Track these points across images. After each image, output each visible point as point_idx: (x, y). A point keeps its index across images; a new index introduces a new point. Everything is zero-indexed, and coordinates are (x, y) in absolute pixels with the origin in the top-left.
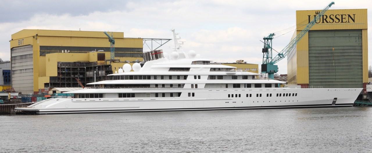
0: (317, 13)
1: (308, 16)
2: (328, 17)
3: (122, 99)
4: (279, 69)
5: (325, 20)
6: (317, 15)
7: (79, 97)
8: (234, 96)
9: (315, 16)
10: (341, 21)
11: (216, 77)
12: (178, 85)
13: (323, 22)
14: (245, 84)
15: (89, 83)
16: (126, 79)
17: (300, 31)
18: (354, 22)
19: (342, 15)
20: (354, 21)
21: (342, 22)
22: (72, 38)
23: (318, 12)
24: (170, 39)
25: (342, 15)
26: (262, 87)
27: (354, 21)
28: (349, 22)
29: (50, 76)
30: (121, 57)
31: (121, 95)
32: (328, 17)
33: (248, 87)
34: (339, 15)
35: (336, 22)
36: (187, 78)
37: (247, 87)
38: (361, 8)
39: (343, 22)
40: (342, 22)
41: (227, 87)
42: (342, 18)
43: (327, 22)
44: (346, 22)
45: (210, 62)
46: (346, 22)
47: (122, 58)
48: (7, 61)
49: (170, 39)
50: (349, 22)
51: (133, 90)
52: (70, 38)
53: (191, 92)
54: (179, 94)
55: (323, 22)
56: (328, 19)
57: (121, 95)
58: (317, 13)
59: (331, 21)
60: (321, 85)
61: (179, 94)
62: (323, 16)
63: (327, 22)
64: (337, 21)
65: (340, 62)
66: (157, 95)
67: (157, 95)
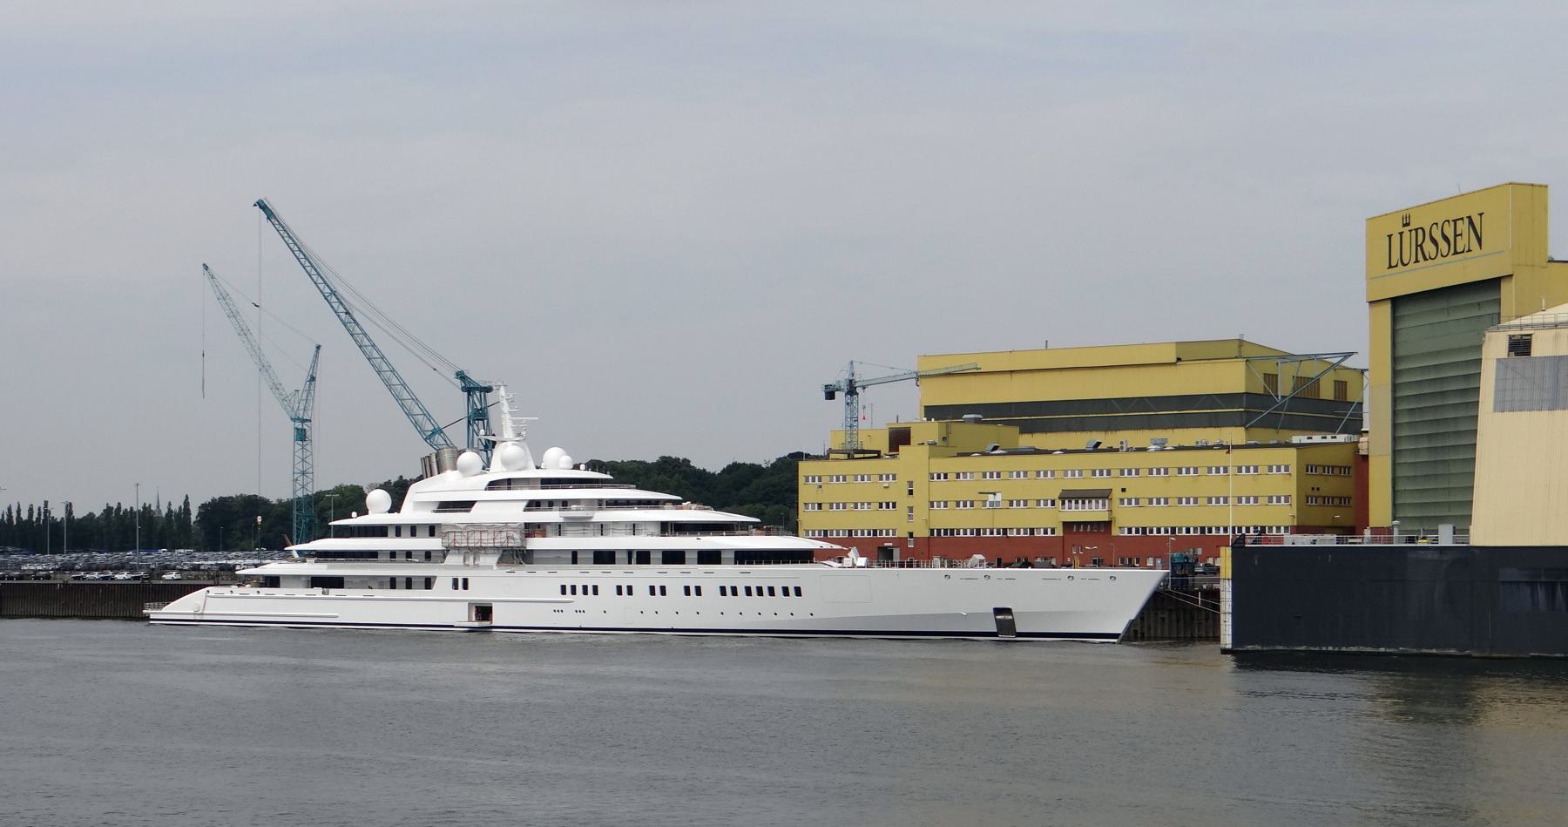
3: (318, 591)
4: (95, 513)
5: (1421, 246)
7: (1083, 566)
8: (579, 590)
9: (1401, 234)
12: (424, 553)
14: (630, 552)
16: (336, 536)
17: (1378, 301)
21: (1456, 253)
22: (1013, 375)
24: (1352, 353)
28: (1469, 250)
30: (1106, 430)
31: (316, 581)
33: (639, 562)
34: (1448, 221)
37: (637, 563)
41: (575, 561)
42: (1456, 236)
44: (1463, 252)
45: (846, 456)
46: (1463, 252)
47: (1104, 433)
49: (1352, 353)
51: (329, 568)
52: (1008, 376)
53: (461, 575)
54: (428, 583)
56: (1429, 247)
57: (316, 581)
61: (428, 583)
65: (1459, 432)
66: (393, 583)
67: (393, 583)
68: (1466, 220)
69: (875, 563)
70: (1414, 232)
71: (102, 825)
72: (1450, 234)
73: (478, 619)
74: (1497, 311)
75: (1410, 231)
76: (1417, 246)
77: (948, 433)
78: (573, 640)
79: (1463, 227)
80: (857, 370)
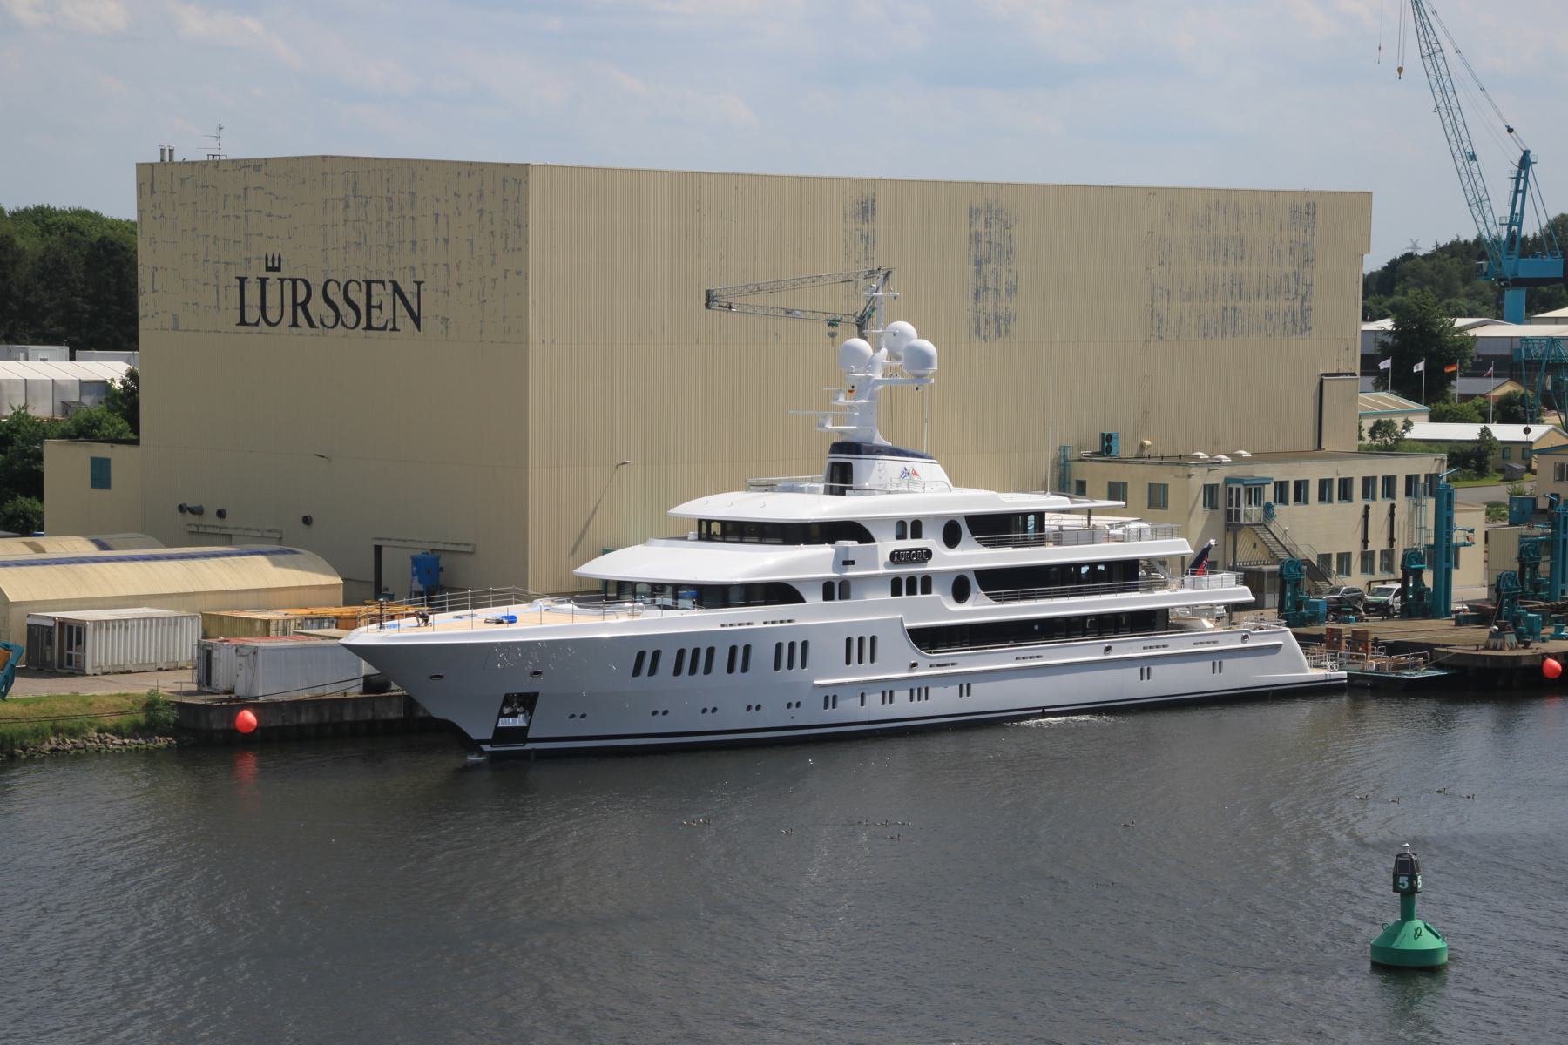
0: (270, 265)
1: (238, 282)
2: (317, 293)
6: (273, 276)
9: (263, 281)
11: (874, 451)
13: (295, 324)
15: (321, 587)
18: (419, 330)
19: (369, 283)
20: (417, 320)
21: (369, 327)
23: (276, 257)
25: (369, 283)
26: (852, 594)
27: (417, 320)
28: (394, 329)
29: (108, 491)
32: (317, 293)
34: (383, 283)
35: (343, 323)
36: (724, 494)
38: (930, 178)
39: (247, 320)
40: (369, 327)
42: (369, 307)
44: (384, 328)
46: (384, 328)
48: (77, 207)
50: (394, 329)
55: (295, 324)
56: (317, 307)
58: (270, 265)
60: (989, 545)
62: (294, 281)
64: (350, 317)
68: (389, 287)
69: (109, 382)
70: (288, 285)
71: (1378, 45)
72: (359, 298)
73: (834, 572)
74: (259, 622)
75: (282, 280)
76: (295, 304)
77: (1470, 174)
78: (250, 639)
79: (381, 294)
80: (1513, 176)
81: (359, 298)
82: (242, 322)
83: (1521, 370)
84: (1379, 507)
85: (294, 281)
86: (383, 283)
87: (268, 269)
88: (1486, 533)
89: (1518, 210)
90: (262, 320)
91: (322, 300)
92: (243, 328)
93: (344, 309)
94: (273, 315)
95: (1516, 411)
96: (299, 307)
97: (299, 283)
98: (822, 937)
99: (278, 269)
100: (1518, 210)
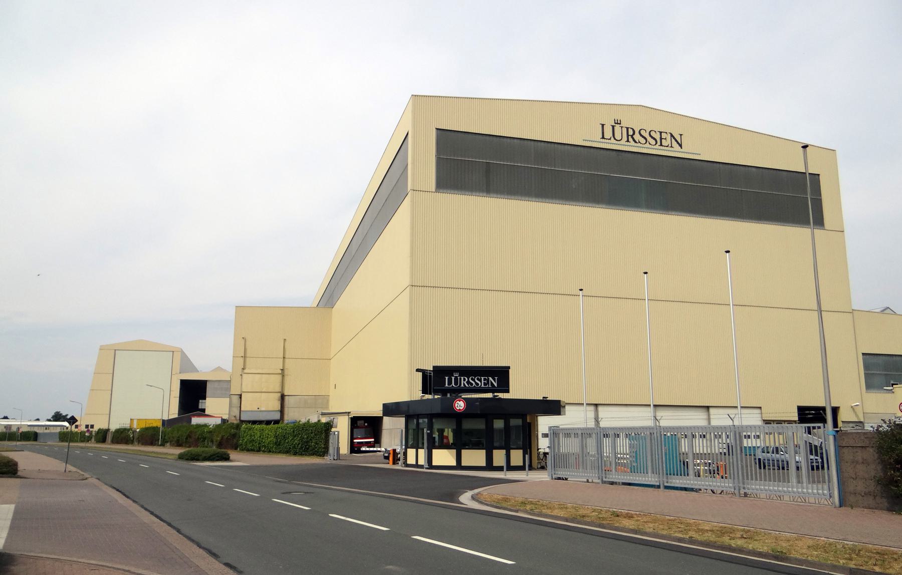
9: (613, 127)
10: (659, 143)
13: (628, 141)
20: (681, 146)
21: (661, 145)
27: (681, 146)
28: (671, 147)
40: (661, 145)
42: (661, 139)
43: (636, 142)
46: (668, 146)
50: (671, 147)
55: (628, 141)
58: (616, 122)
59: (643, 141)
63: (636, 142)
70: (625, 130)
72: (657, 137)
76: (628, 135)
81: (657, 137)
82: (603, 138)
83: (820, 478)
84: (772, 436)
85: (627, 129)
86: (666, 133)
87: (615, 123)
88: (835, 150)
89: (527, 456)
90: (612, 138)
91: (639, 136)
92: (603, 140)
93: (649, 139)
94: (618, 137)
95: (893, 461)
96: (630, 137)
97: (629, 129)
98: (860, 459)
99: (620, 124)
100: (527, 456)
